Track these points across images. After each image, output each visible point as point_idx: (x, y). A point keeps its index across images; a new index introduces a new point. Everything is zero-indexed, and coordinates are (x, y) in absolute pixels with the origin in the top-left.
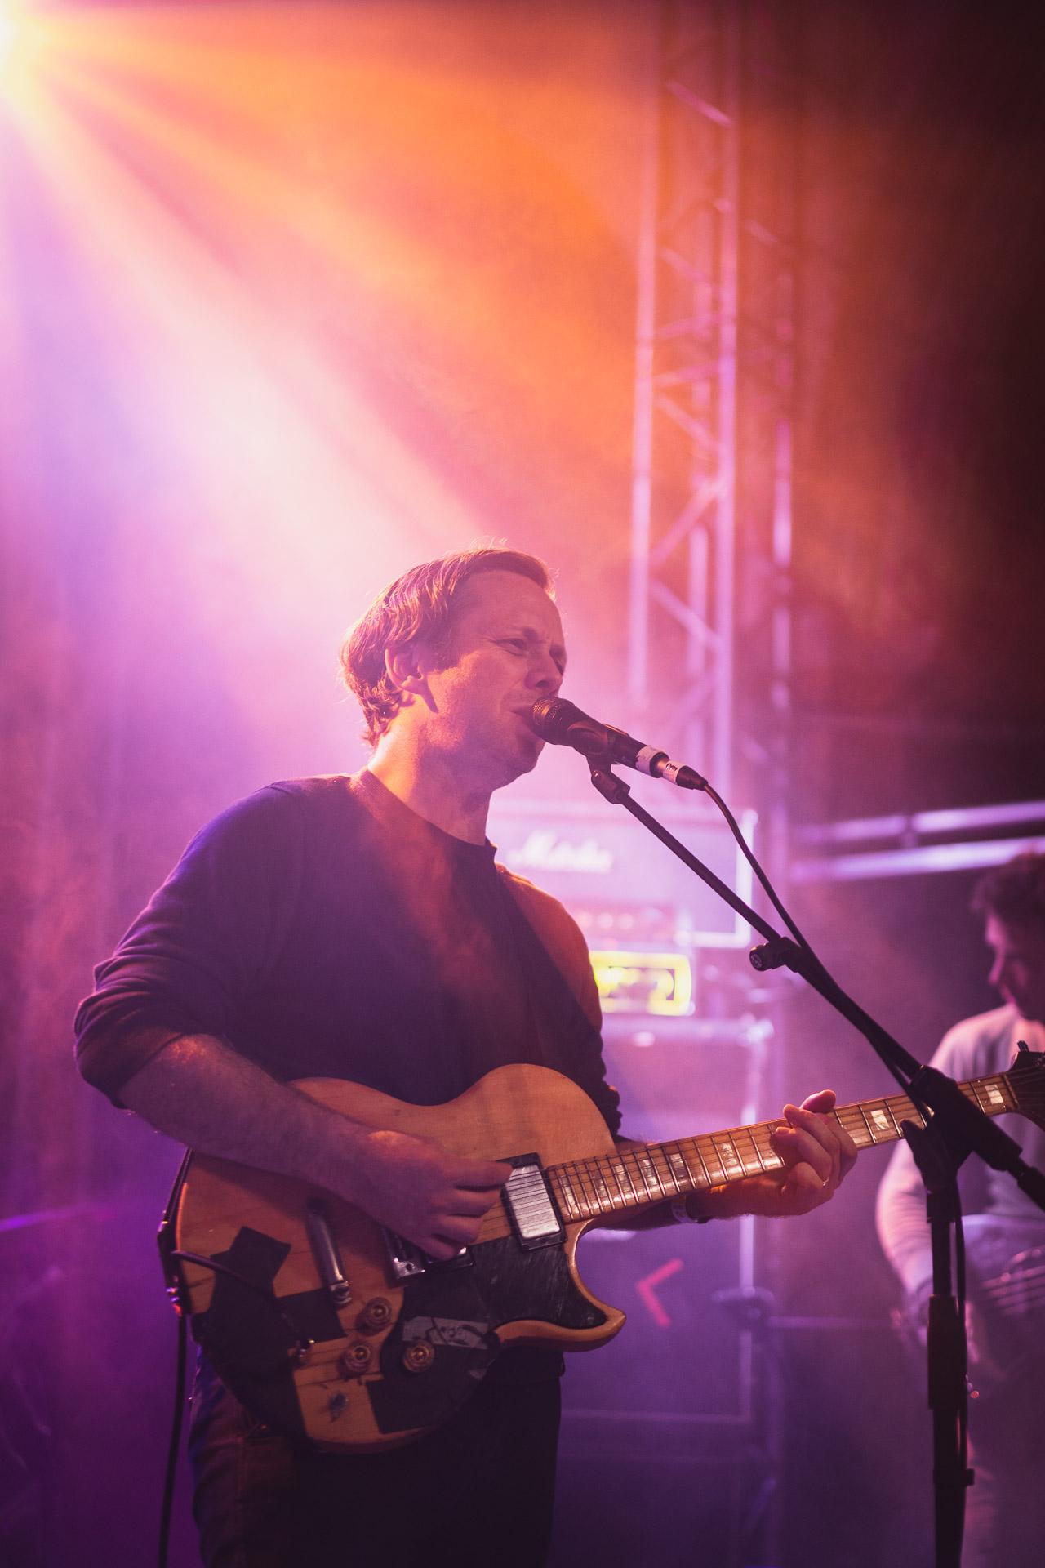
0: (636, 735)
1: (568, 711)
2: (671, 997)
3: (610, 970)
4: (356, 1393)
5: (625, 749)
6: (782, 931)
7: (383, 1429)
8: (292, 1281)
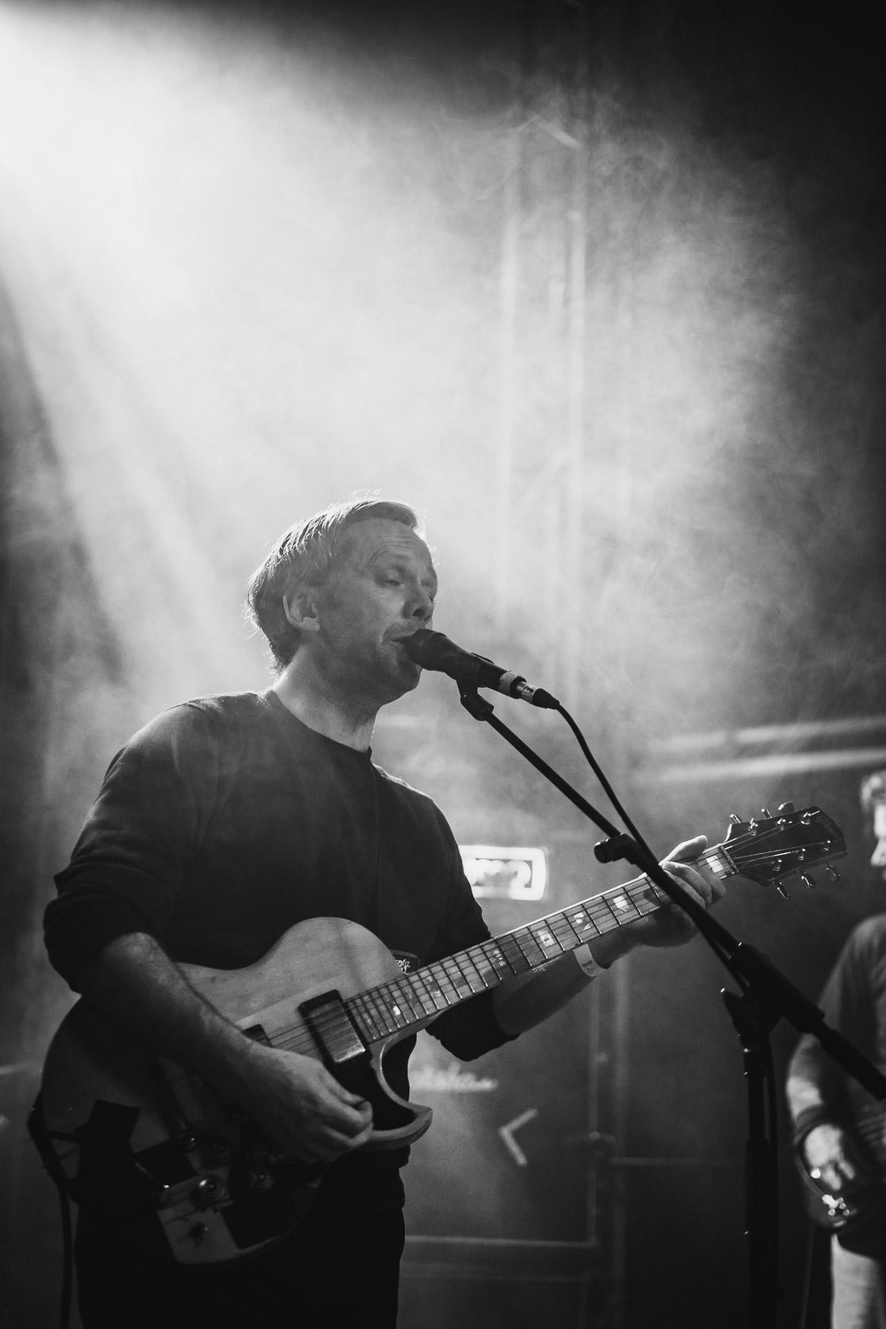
0: (499, 663)
1: (440, 640)
2: (528, 885)
3: (477, 863)
4: (211, 1220)
5: (488, 674)
6: (623, 829)
7: (241, 1245)
8: (149, 1133)
